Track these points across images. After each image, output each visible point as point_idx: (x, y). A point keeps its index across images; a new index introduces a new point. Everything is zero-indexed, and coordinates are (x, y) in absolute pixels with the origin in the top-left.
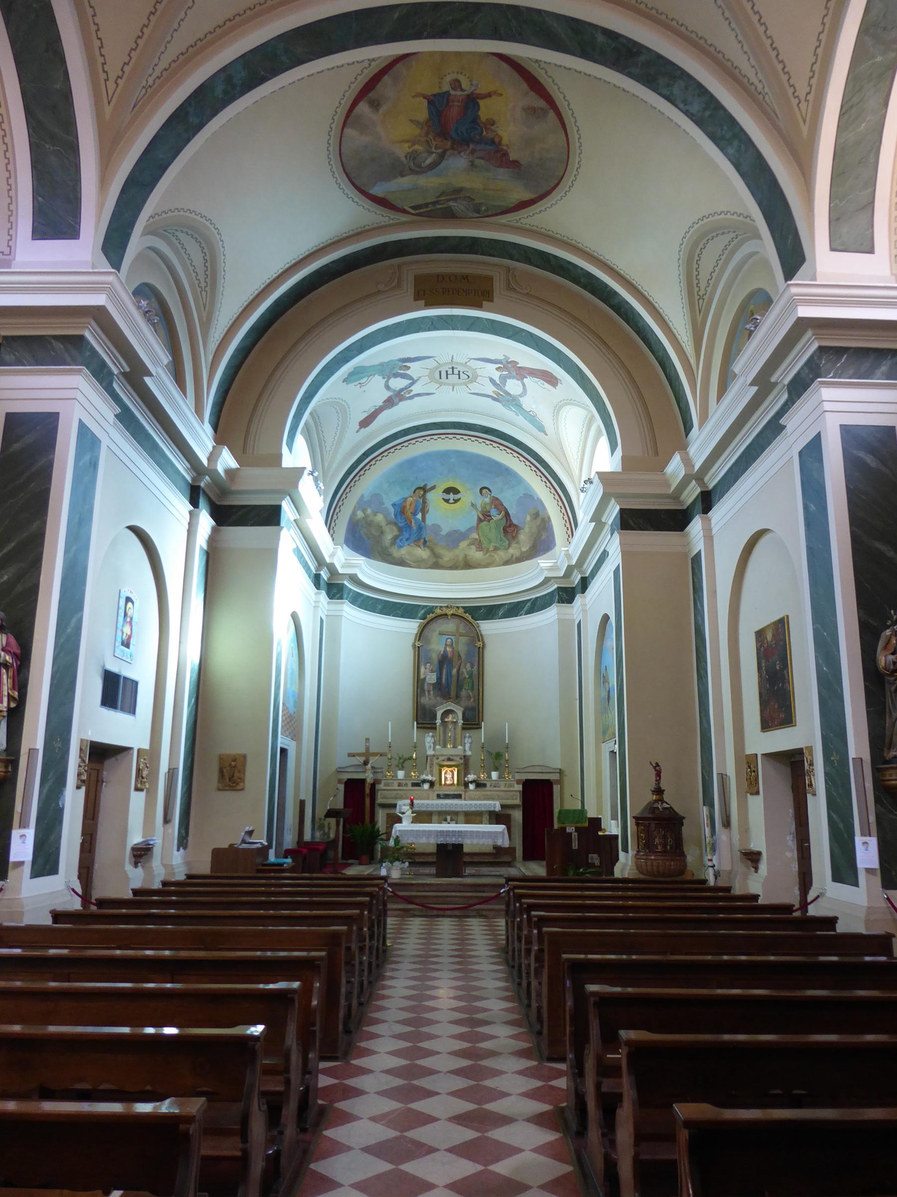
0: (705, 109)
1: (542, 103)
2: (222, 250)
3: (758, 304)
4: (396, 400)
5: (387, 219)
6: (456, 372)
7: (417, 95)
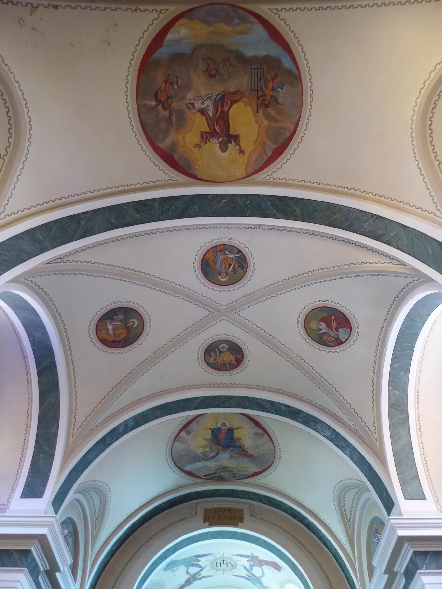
0: (332, 435)
1: (261, 431)
2: (110, 498)
3: (377, 528)
4: (192, 580)
5: (191, 481)
6: (225, 562)
7: (207, 429)
